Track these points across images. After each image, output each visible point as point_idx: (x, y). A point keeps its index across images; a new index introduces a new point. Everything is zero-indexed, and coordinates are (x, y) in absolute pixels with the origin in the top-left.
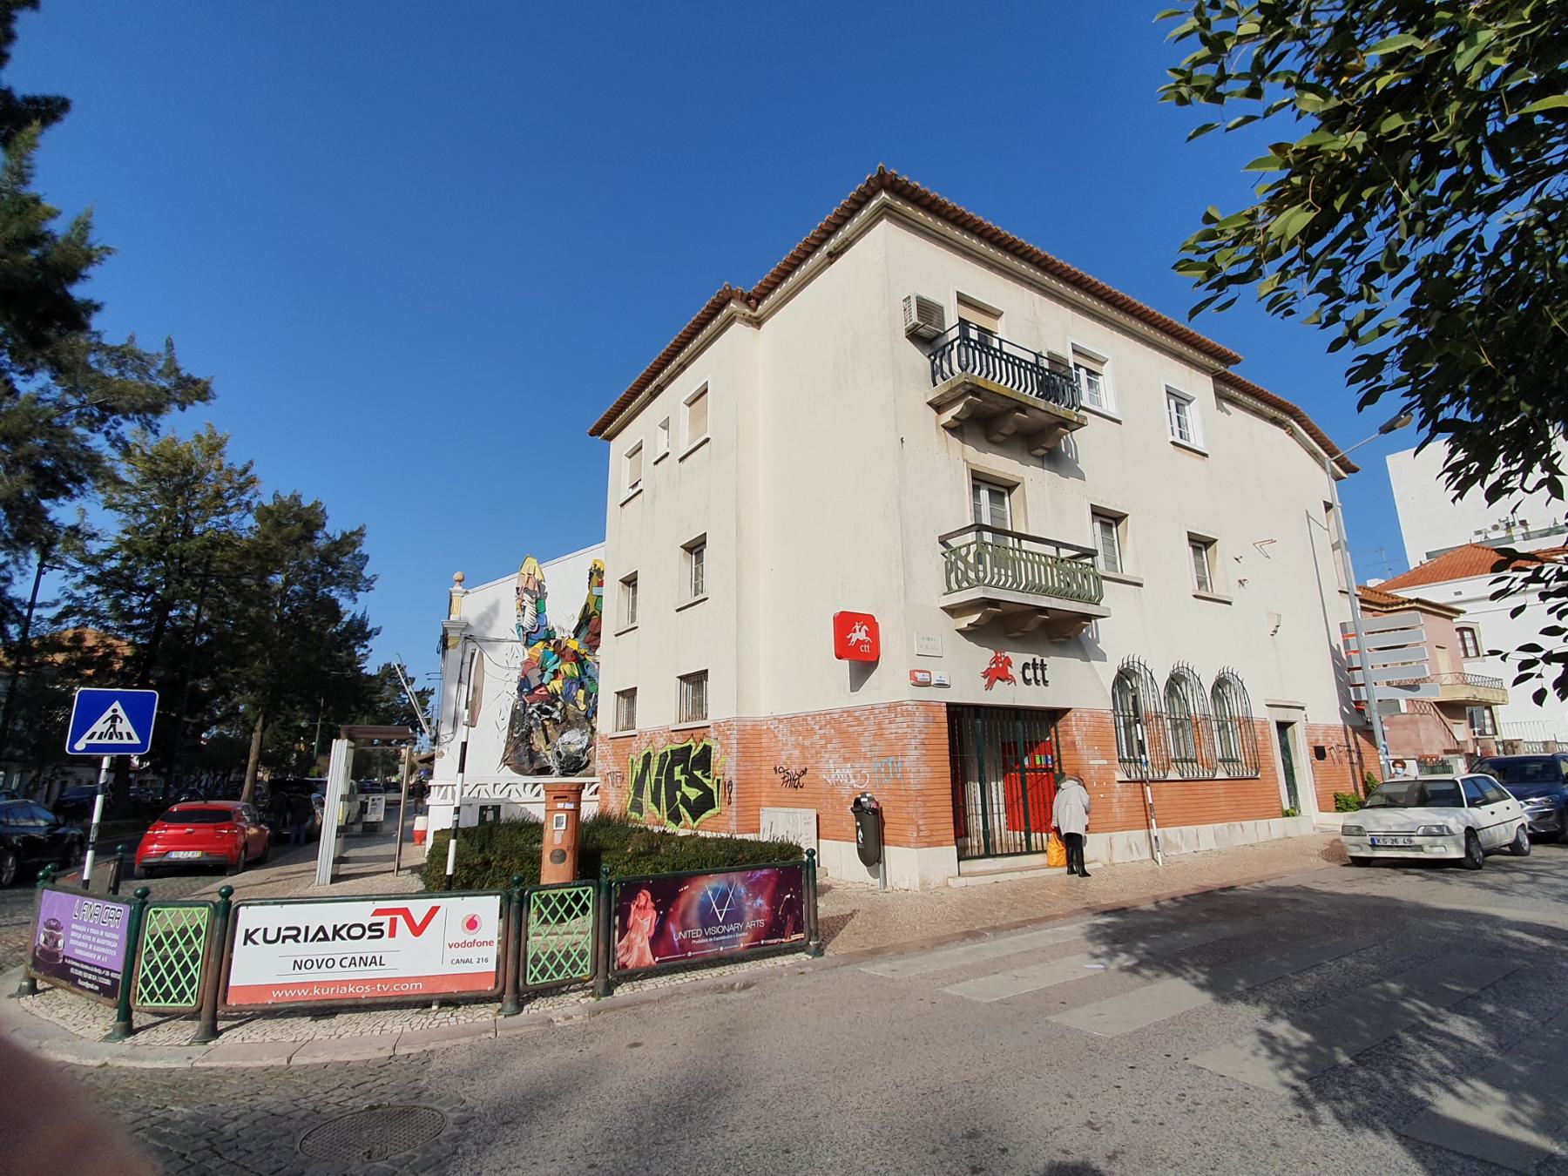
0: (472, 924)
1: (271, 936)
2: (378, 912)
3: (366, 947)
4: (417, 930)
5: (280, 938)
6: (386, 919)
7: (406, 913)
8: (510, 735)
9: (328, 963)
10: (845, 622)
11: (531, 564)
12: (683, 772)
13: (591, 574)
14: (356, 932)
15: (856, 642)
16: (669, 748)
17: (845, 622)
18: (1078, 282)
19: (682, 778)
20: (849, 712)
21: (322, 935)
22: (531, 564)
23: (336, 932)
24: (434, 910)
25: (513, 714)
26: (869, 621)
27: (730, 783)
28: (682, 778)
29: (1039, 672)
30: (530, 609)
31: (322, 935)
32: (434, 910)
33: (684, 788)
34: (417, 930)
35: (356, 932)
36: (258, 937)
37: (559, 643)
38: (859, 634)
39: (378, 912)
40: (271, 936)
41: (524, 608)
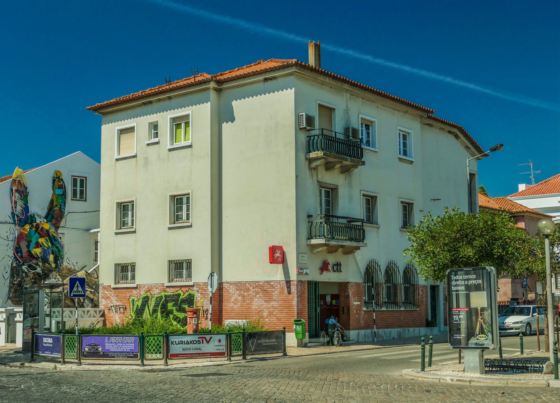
0: (220, 341)
1: (177, 343)
2: (199, 338)
3: (197, 346)
4: (208, 342)
5: (179, 343)
6: (201, 339)
7: (205, 338)
8: (11, 282)
9: (190, 349)
10: (273, 250)
11: (17, 171)
12: (174, 305)
13: (54, 181)
14: (195, 342)
15: (276, 255)
16: (163, 294)
17: (273, 250)
18: (379, 94)
19: (174, 308)
20: (268, 282)
21: (187, 343)
22: (17, 171)
23: (191, 342)
24: (211, 337)
25: (12, 269)
26: (281, 248)
27: (207, 310)
28: (174, 308)
29: (339, 267)
30: (20, 203)
31: (187, 343)
32: (211, 337)
33: (175, 313)
34: (208, 342)
35: (195, 342)
36: (174, 343)
37: (38, 225)
38: (278, 254)
39: (199, 338)
40: (177, 343)
41: (16, 203)
